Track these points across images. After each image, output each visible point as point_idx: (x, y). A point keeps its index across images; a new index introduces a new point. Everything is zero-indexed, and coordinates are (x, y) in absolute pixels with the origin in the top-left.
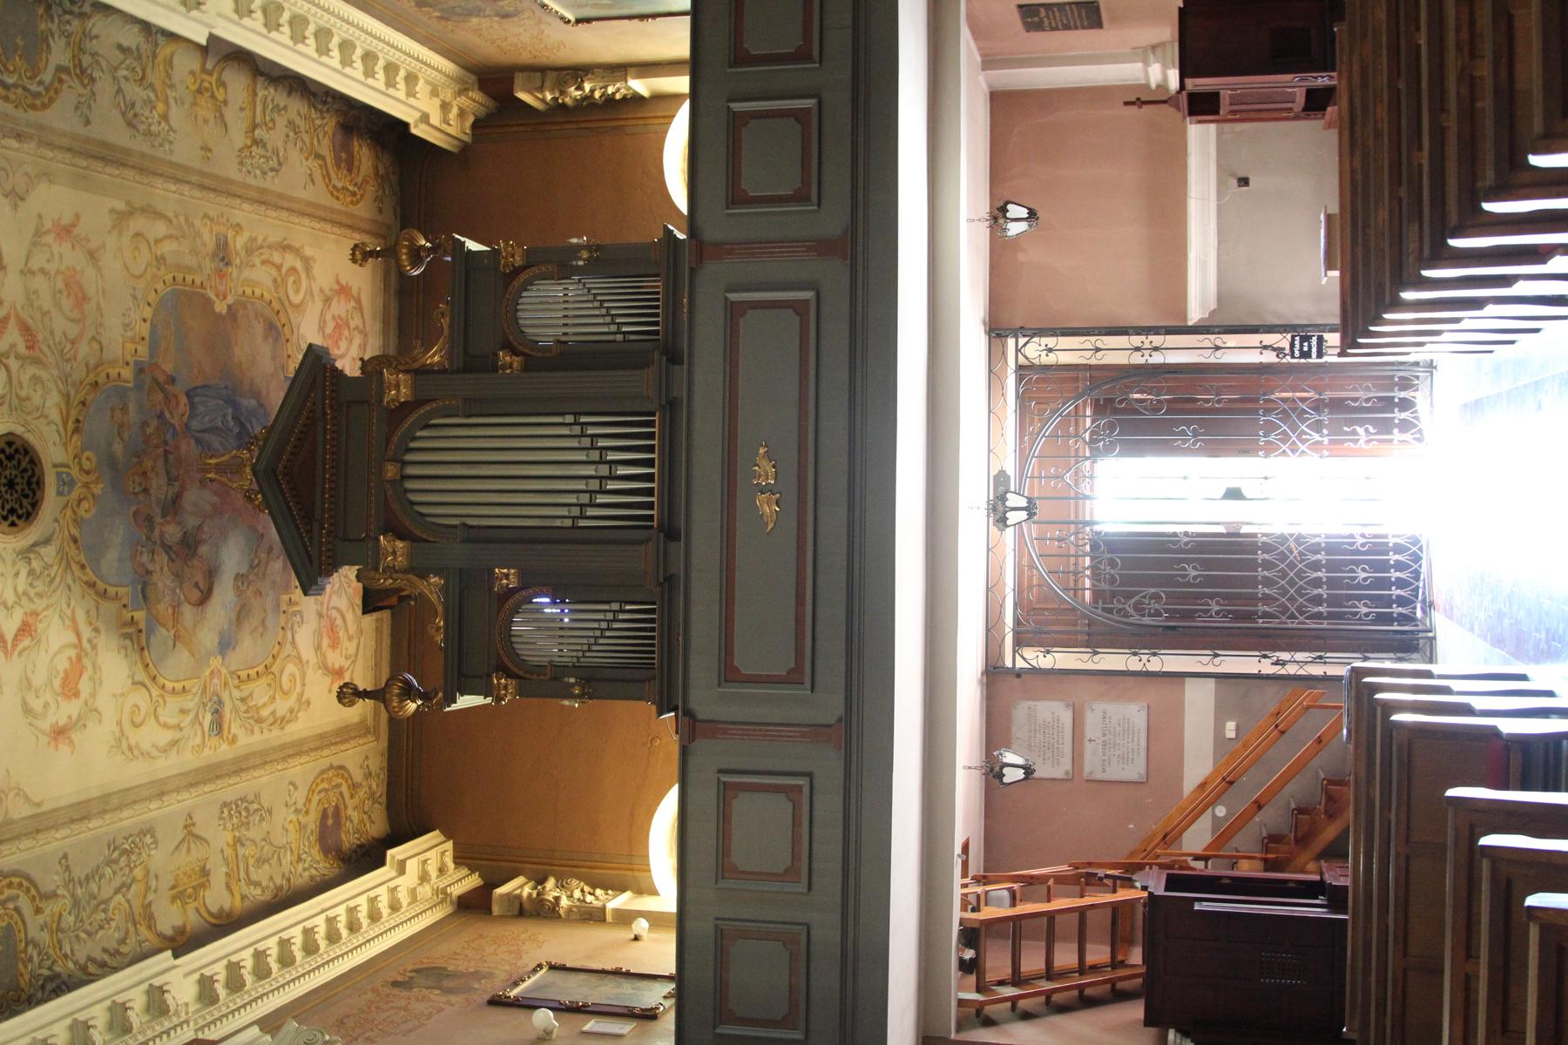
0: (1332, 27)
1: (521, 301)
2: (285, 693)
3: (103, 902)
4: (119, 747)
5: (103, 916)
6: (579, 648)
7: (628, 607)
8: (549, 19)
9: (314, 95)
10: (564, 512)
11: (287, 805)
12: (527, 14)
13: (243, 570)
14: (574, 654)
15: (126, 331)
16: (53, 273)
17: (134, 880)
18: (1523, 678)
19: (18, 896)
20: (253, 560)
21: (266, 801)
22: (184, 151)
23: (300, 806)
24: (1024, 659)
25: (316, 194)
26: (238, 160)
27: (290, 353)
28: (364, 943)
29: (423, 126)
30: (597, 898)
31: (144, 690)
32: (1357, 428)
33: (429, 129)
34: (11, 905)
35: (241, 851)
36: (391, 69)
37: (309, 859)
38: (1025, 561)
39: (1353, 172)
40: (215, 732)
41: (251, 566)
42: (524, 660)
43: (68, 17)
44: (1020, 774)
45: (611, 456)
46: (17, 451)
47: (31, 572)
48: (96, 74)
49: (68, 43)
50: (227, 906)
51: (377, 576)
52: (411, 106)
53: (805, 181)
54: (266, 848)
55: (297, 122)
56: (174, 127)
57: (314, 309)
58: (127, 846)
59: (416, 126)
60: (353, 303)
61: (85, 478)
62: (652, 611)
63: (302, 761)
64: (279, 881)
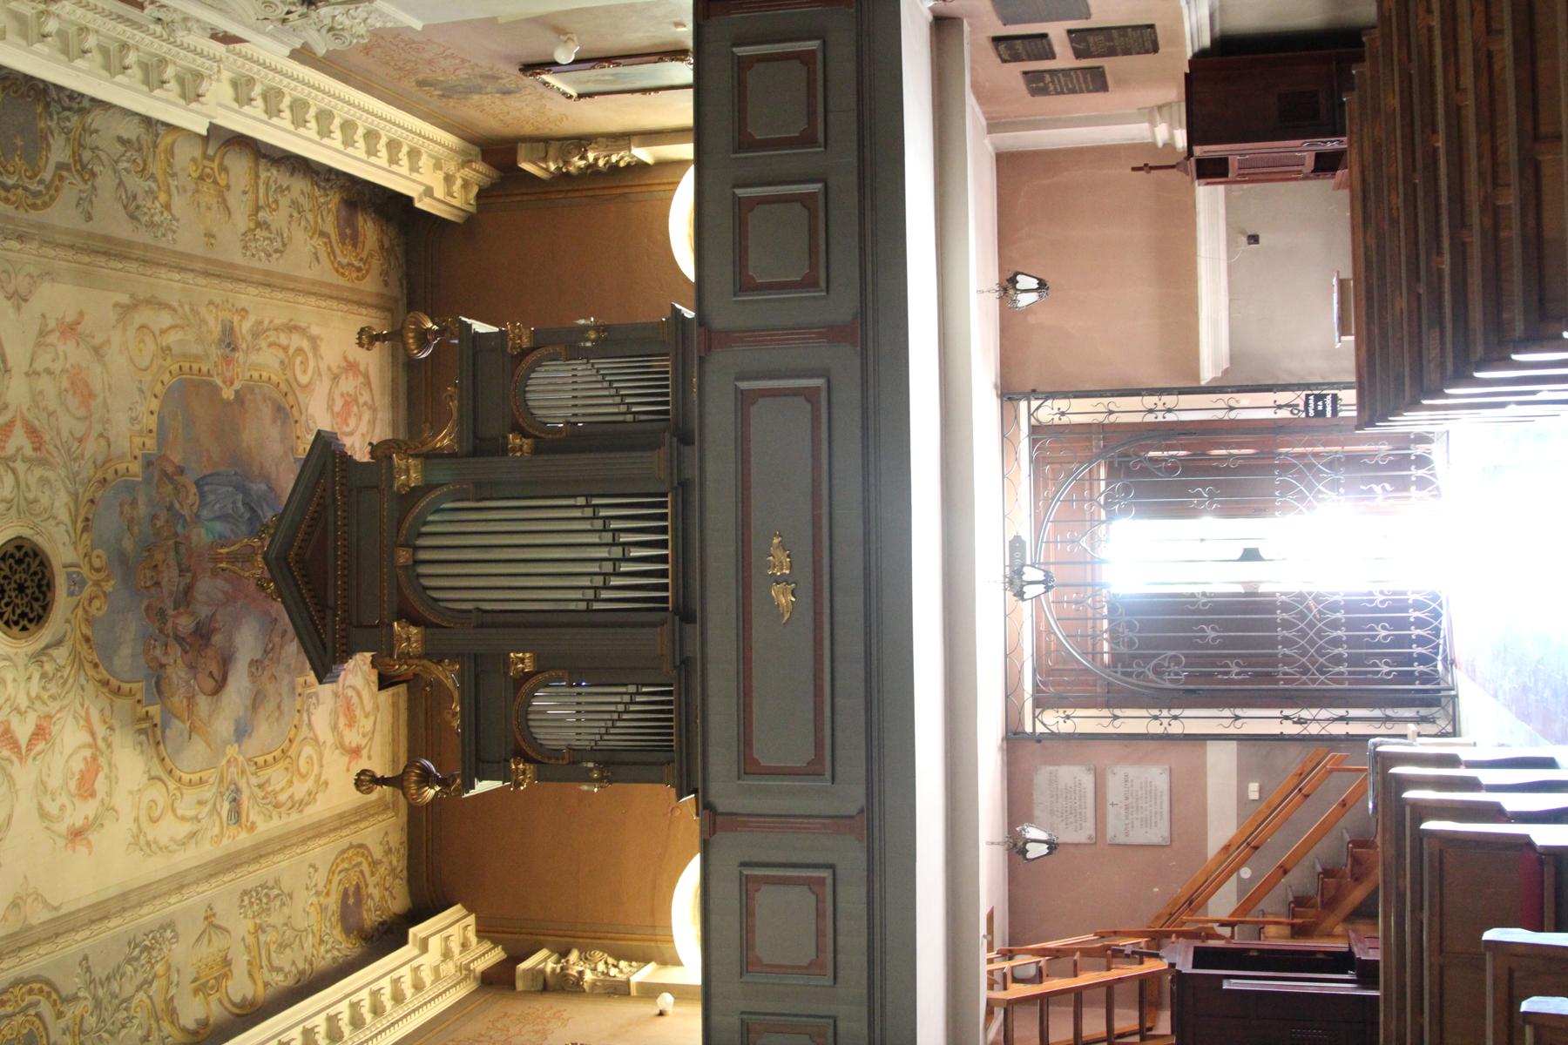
0: (1340, 98)
1: (530, 382)
2: (303, 776)
3: (125, 1000)
4: (137, 844)
5: (125, 1014)
6: (596, 731)
7: (645, 690)
8: (548, 93)
9: (318, 174)
10: (577, 595)
11: (307, 888)
12: (528, 91)
13: (257, 657)
14: (592, 737)
15: (133, 424)
16: (57, 372)
17: (155, 976)
18: (1549, 763)
19: (39, 1002)
20: (267, 645)
21: (286, 885)
22: (187, 239)
23: (320, 887)
24: (1045, 725)
25: (323, 272)
26: (243, 243)
27: (299, 434)
28: (389, 1027)
29: (427, 200)
30: (621, 971)
31: (160, 784)
32: (1374, 486)
33: (434, 203)
34: (32, 1012)
35: (263, 938)
36: (393, 146)
37: (331, 940)
38: (1043, 628)
39: (1367, 248)
40: (233, 821)
41: (265, 651)
42: (541, 744)
43: (67, 113)
44: (1044, 849)
45: (624, 538)
46: (26, 554)
47: (44, 676)
48: (96, 169)
49: (68, 140)
50: (250, 996)
51: (392, 663)
52: (414, 181)
53: (813, 266)
54: (288, 933)
55: (300, 201)
56: (178, 215)
57: (322, 388)
58: (147, 943)
59: (420, 200)
60: (361, 379)
61: (96, 576)
62: (669, 693)
63: (321, 842)
64: (301, 965)
